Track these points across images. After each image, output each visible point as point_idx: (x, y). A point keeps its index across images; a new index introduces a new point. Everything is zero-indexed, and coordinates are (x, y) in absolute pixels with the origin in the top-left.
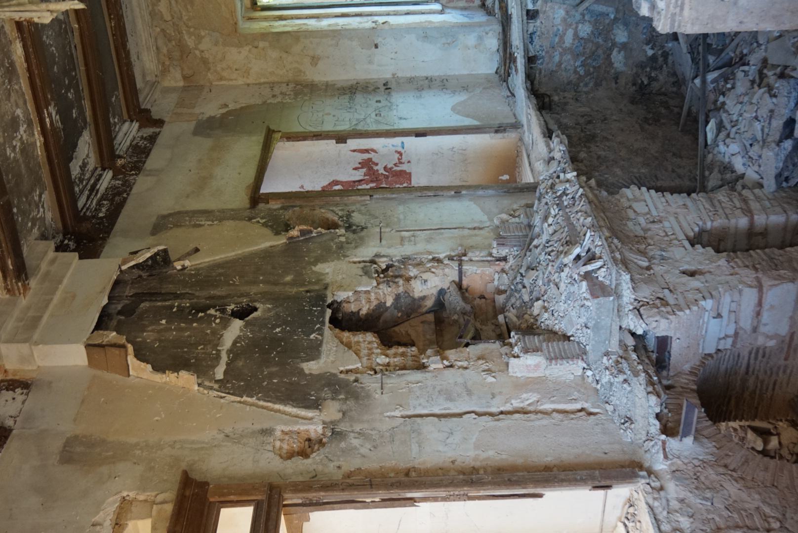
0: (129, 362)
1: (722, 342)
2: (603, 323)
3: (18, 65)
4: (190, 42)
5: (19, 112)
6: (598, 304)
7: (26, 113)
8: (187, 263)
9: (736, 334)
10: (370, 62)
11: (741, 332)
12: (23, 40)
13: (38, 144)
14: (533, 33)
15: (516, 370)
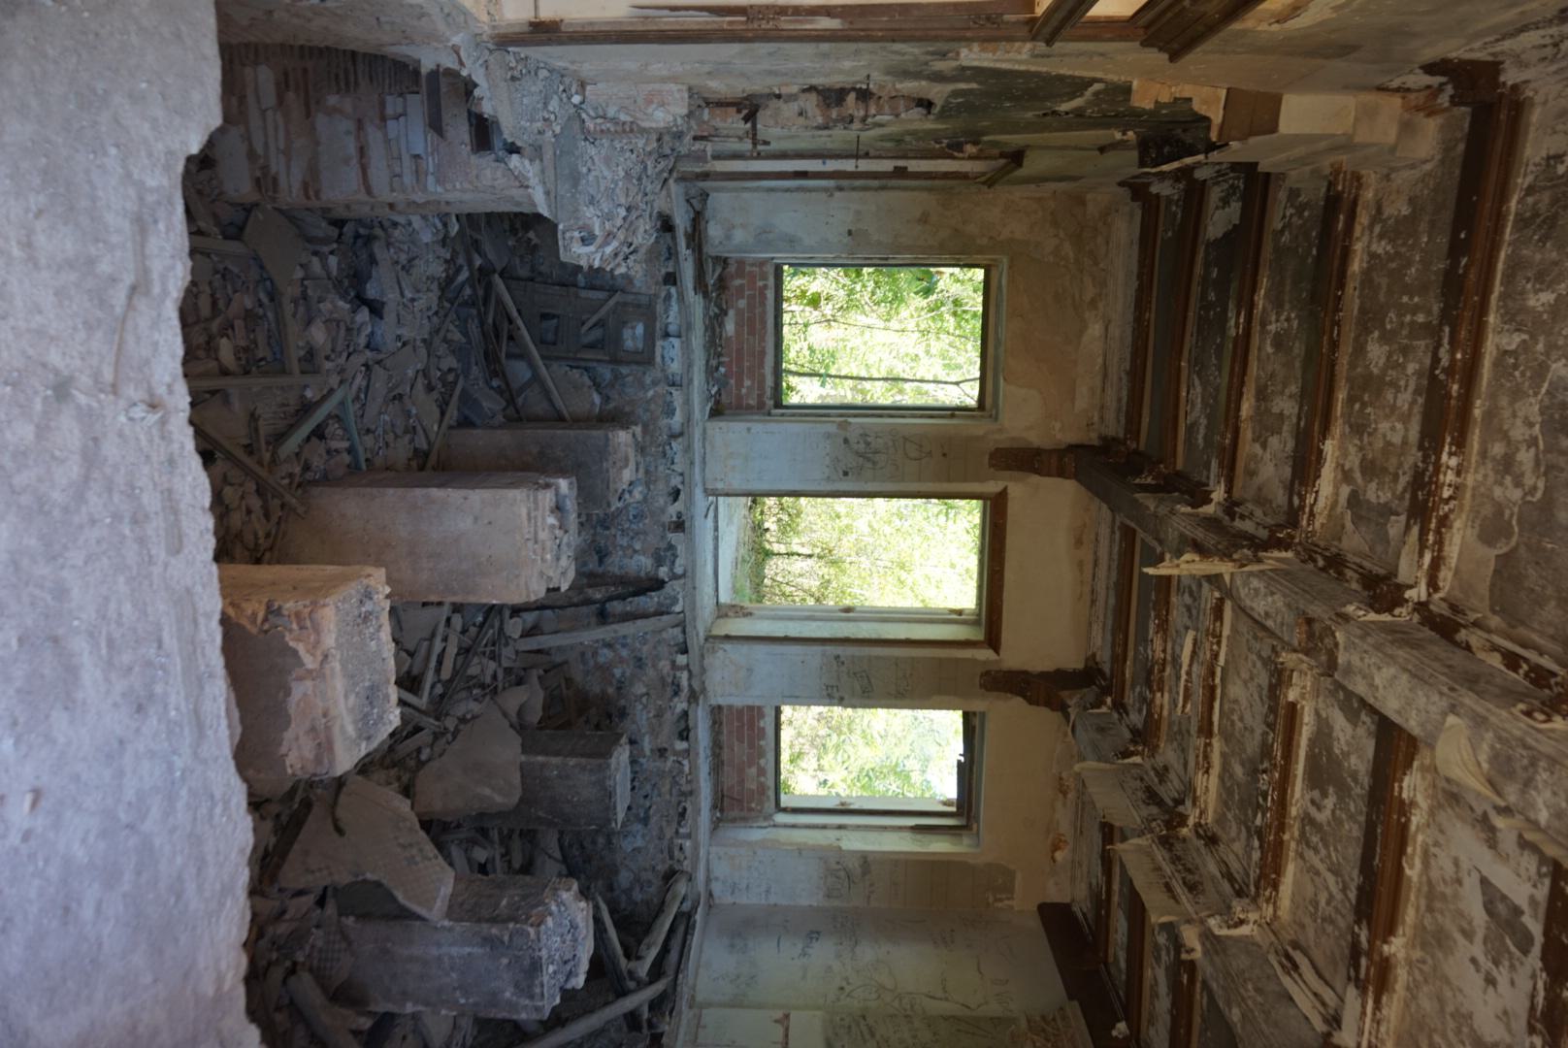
0: (1221, 112)
1: (400, 110)
2: (567, 186)
3: (1253, 392)
4: (1068, 249)
5: (1270, 350)
6: (578, 219)
7: (1262, 341)
8: (1118, 136)
9: (383, 119)
10: (858, 213)
11: (377, 122)
12: (1237, 417)
13: (1263, 292)
14: (668, 259)
15: (677, 96)
